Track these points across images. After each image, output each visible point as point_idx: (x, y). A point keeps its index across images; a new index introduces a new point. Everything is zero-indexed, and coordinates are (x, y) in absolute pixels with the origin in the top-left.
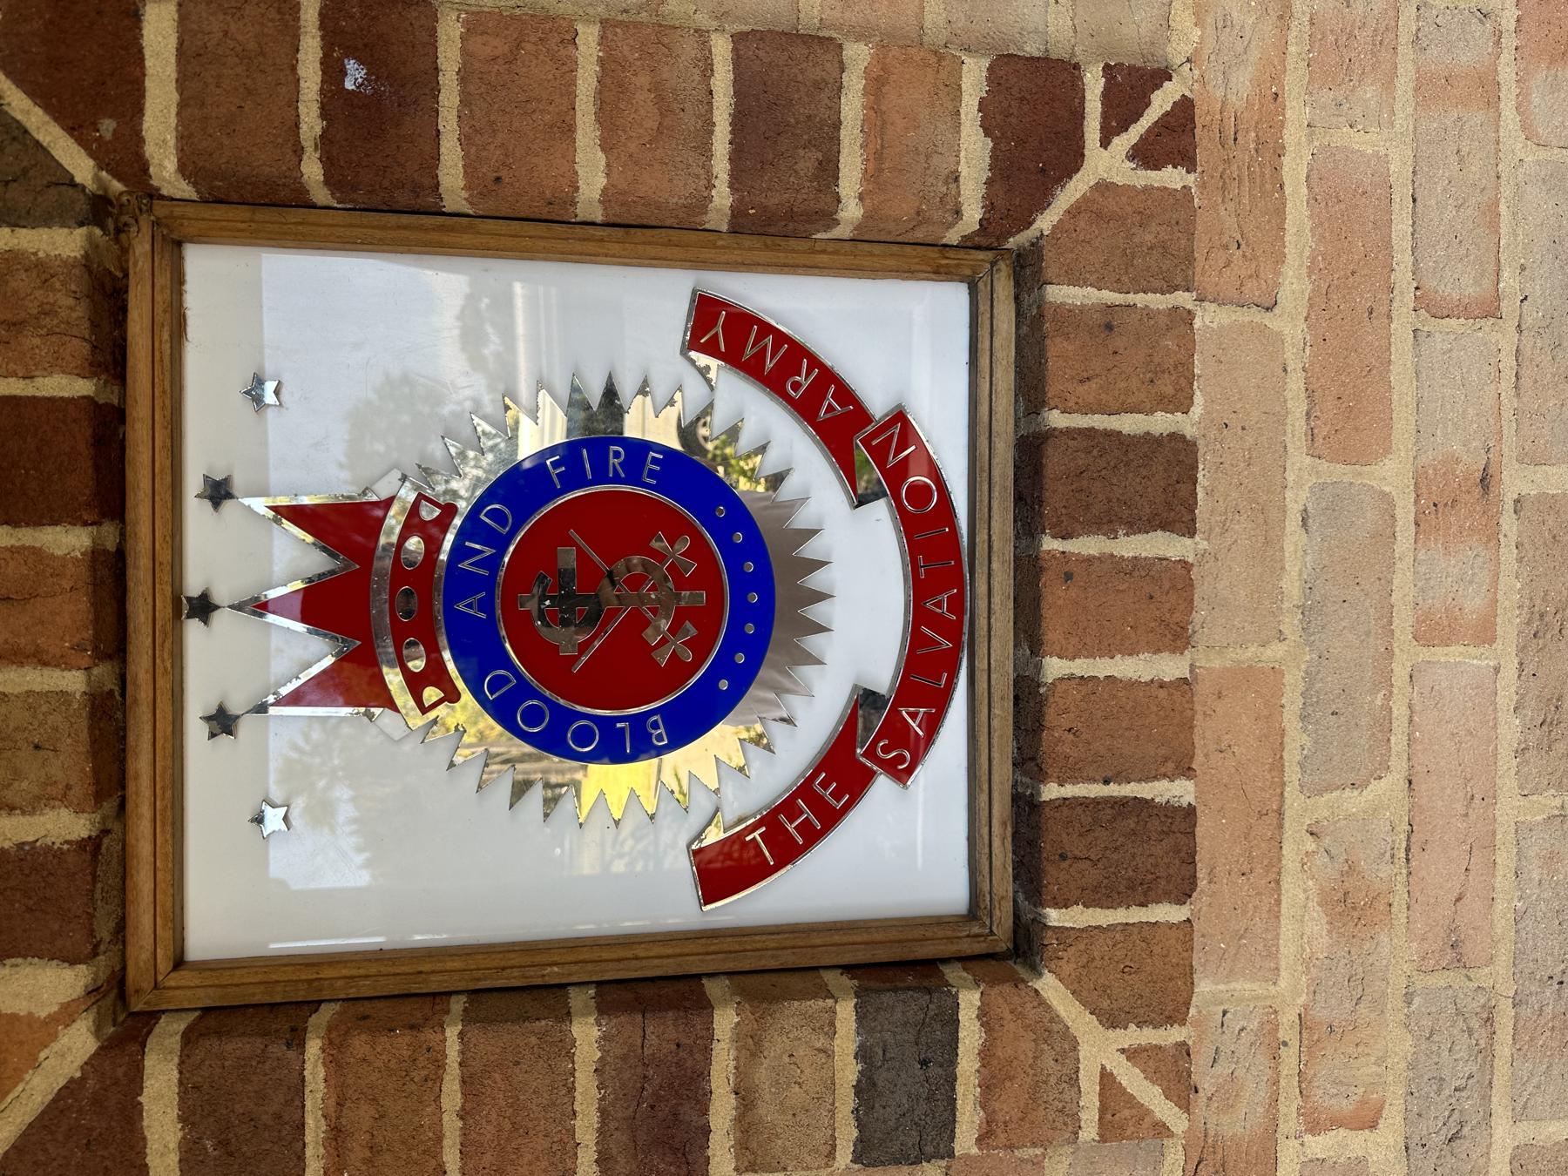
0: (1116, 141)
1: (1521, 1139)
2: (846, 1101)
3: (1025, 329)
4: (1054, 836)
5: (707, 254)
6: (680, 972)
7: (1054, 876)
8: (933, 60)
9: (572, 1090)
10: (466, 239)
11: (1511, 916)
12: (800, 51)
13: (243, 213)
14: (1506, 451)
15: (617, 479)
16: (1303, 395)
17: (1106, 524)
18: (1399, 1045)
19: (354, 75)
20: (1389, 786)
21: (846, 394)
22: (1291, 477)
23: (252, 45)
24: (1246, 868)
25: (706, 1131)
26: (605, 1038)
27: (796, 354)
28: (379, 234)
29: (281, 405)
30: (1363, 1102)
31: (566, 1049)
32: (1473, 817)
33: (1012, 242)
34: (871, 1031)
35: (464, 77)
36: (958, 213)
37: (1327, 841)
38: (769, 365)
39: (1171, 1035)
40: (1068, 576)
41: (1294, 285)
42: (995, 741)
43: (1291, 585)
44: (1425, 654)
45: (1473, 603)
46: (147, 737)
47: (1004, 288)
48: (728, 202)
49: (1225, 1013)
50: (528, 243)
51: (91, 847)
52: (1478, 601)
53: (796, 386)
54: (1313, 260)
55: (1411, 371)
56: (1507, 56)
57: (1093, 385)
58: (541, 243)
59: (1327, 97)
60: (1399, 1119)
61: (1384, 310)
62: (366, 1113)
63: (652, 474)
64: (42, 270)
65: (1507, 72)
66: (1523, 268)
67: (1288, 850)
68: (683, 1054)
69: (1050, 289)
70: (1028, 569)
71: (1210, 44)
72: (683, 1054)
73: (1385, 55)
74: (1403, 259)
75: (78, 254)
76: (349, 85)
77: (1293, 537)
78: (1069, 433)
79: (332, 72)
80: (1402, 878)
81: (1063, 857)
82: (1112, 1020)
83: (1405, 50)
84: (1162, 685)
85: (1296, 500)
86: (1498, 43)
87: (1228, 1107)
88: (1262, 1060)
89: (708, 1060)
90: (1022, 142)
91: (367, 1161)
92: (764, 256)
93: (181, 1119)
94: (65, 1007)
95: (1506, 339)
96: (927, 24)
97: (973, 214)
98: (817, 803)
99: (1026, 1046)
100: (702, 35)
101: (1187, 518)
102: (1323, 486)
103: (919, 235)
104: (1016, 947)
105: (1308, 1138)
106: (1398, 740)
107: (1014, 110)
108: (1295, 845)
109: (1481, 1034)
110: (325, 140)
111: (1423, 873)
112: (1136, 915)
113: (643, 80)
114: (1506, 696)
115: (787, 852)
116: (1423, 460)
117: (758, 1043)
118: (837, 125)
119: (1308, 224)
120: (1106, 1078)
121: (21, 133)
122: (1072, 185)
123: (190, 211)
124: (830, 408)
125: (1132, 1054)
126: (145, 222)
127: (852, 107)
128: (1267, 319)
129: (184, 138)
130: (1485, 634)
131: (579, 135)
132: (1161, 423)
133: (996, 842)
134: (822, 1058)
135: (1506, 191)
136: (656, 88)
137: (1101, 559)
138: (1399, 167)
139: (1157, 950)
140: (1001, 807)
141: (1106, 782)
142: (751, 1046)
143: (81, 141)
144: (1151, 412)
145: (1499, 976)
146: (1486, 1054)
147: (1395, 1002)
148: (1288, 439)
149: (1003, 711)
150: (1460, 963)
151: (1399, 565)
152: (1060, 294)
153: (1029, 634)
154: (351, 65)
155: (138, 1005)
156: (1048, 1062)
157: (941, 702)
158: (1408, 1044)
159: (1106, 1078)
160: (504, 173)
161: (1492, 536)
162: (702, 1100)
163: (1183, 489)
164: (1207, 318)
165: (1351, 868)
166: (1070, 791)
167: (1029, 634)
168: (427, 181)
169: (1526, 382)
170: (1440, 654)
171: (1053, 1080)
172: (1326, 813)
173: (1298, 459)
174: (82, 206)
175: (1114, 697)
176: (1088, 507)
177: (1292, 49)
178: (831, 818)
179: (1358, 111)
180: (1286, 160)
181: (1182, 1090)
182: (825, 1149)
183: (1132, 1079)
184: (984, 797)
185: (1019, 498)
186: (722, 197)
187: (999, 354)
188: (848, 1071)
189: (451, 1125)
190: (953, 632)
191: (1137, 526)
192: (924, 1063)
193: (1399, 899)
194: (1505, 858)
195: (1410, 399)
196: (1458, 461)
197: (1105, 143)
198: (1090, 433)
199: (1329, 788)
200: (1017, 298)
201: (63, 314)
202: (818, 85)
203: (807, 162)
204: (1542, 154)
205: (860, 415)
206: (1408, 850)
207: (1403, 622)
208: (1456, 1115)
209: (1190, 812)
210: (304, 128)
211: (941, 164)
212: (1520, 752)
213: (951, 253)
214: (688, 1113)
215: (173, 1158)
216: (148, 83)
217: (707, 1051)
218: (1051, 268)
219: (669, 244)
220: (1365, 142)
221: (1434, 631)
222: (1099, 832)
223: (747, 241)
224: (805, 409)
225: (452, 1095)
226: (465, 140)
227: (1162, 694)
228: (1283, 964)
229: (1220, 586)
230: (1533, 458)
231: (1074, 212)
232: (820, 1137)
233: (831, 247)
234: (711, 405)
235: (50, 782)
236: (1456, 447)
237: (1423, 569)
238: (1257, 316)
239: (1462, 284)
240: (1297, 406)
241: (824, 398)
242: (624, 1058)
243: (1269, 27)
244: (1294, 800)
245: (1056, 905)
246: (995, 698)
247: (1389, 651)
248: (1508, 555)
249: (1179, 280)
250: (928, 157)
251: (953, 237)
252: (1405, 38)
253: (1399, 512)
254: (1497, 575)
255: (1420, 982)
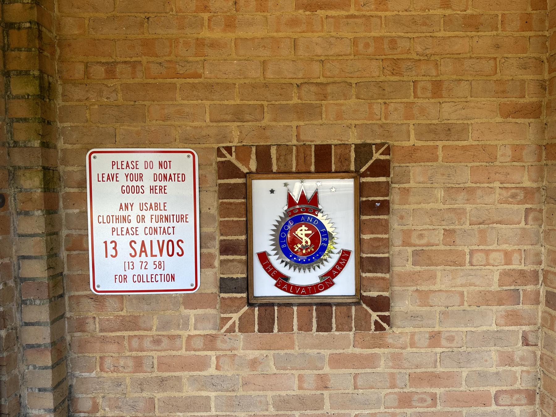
0: (378, 317)
1: (212, 398)
2: (230, 276)
3: (348, 304)
4: (269, 309)
5: (357, 253)
6: (248, 250)
7: (263, 309)
8: (388, 287)
9: (235, 236)
10: (357, 218)
11: (251, 394)
12: (387, 267)
13: (359, 188)
14: (332, 391)
15: (322, 239)
16: (339, 352)
17: (318, 317)
18: (229, 374)
19: (378, 204)
20: (275, 370)
21: (337, 275)
22: (326, 350)
23: (381, 191)
24: (261, 344)
25: (227, 255)
26: (242, 240)
27: (343, 267)
28: (357, 206)
29: (335, 228)
30: (220, 367)
31: (241, 235)
32: (269, 386)
33: (361, 301)
34: (241, 280)
35: (379, 219)
36: (365, 292)
37: (265, 358)
38: (341, 263)
39: (237, 329)
40: (309, 311)
41: (358, 351)
42: (282, 300)
43: (308, 351)
44: (296, 376)
45: (305, 385)
46: (285, 176)
47: (354, 300)
48: (364, 256)
49: (237, 340)
50: (357, 227)
51: (272, 171)
52: (305, 386)
53: (337, 267)
54: (362, 354)
55: (344, 373)
56: (399, 390)
57: (340, 314)
58: (357, 228)
59: (389, 356)
60: (217, 374)
61: (354, 367)
62: (233, 207)
63: (323, 245)
64: (349, 165)
65: (396, 390)
66: (363, 394)
67: (264, 351)
68: (239, 251)
69: (354, 307)
70: (311, 305)
71: (396, 335)
72: (239, 251)
73: (397, 367)
74: (363, 371)
75: (351, 169)
76: (376, 204)
77: (316, 351)
78: (332, 310)
79: (378, 201)
80: (258, 373)
81: (266, 310)
82: (240, 319)
83: (398, 371)
84: (293, 326)
85: (322, 351)
86: (401, 388)
87: (222, 341)
88: (229, 348)
89: (238, 255)
90: (376, 302)
91: (227, 208)
92: (357, 261)
93: (234, 183)
94: (250, 169)
95: (350, 391)
96: (394, 287)
97: (365, 294)
98: (337, 270)
99: (237, 305)
100: (388, 252)
101: (319, 330)
102: (324, 357)
103: (362, 286)
104: (250, 304)
105: (215, 356)
106: (282, 372)
107: (381, 301)
108: (265, 352)
109: (231, 389)
110: (369, 201)
111: (259, 377)
112: (256, 322)
113: (381, 244)
114: (289, 392)
115: (265, 267)
116: (329, 375)
117: (240, 262)
118: (376, 273)
119: (368, 353)
120: (231, 318)
121: (367, 162)
122: (370, 310)
123: (358, 181)
124: (334, 272)
125: (234, 323)
126: (357, 175)
127: (379, 275)
128: (352, 346)
129: (368, 182)
130: (300, 388)
131: (372, 235)
132: (334, 326)
133: (266, 300)
134: (237, 272)
135: (376, 390)
136: (380, 246)
137: (312, 316)
138: (379, 370)
139: (251, 326)
140: (272, 301)
141: (277, 317)
142: (240, 261)
143: (366, 170)
144: (336, 324)
145: (241, 393)
146: (227, 391)
147: (237, 372)
148: (332, 350)
149: (287, 301)
150: (243, 385)
151: (311, 371)
152: (353, 308)
153: (299, 305)
154: (379, 204)
155: (247, 175)
156: (234, 308)
157: (288, 291)
158: (230, 375)
159: (231, 318)
160: (365, 225)
161: (317, 389)
162: (232, 254)
163: (324, 330)
164: (351, 333)
165: (260, 363)
166: (276, 311)
167: (299, 305)
168: (364, 214)
169: (343, 395)
170: (297, 379)
171: (231, 309)
172: (270, 358)
173: (329, 352)
174: (358, 170)
175: (291, 318)
176: (320, 314)
177: (397, 350)
178: (270, 273)
179: (387, 362)
180: (378, 349)
181: (228, 331)
182: (223, 273)
183: (230, 322)
184: (273, 298)
185: (321, 303)
186: (364, 255)
187: (344, 300)
188: (235, 276)
189: (231, 219)
190: (299, 293)
191: (317, 321)
192: (235, 288)
193: (255, 373)
194: (261, 393)
195: (340, 373)
196: (329, 382)
197: (377, 316)
198: (332, 314)
199: (274, 359)
200: (353, 302)
201: (343, 168)
202: (382, 270)
203: (371, 268)
204: (383, 397)
205: (333, 277)
206: (263, 374)
207: (302, 372)
208: (217, 385)
209: (273, 332)
210: (370, 198)
211: (372, 289)
212: (280, 396)
213: (359, 291)
214: (231, 252)
215: (229, 182)
216: (375, 178)
217: (239, 255)
218: (358, 307)
219: (358, 247)
220: (382, 363)
221: (300, 377)
222: (269, 316)
223: (359, 259)
224: (334, 268)
225: (235, 219)
226: (370, 219)
227: (291, 326)
228: (245, 351)
229: (308, 338)
230: (330, 397)
231: (366, 310)
232: (225, 272)
233: (359, 272)
234: (334, 253)
235: (280, 167)
236: (332, 381)
237: (311, 376)
238: (352, 344)
239: (360, 382)
240: (338, 351)
241: (336, 271)
242: (239, 243)
243: (400, 345)
244: (272, 352)
245: (258, 309)
246: (289, 300)
247: (297, 370)
248: (313, 392)
249: (357, 328)
250: (373, 287)
251: (362, 292)
252: (401, 370)
253: (320, 371)
254: (310, 390)
255: (240, 377)
